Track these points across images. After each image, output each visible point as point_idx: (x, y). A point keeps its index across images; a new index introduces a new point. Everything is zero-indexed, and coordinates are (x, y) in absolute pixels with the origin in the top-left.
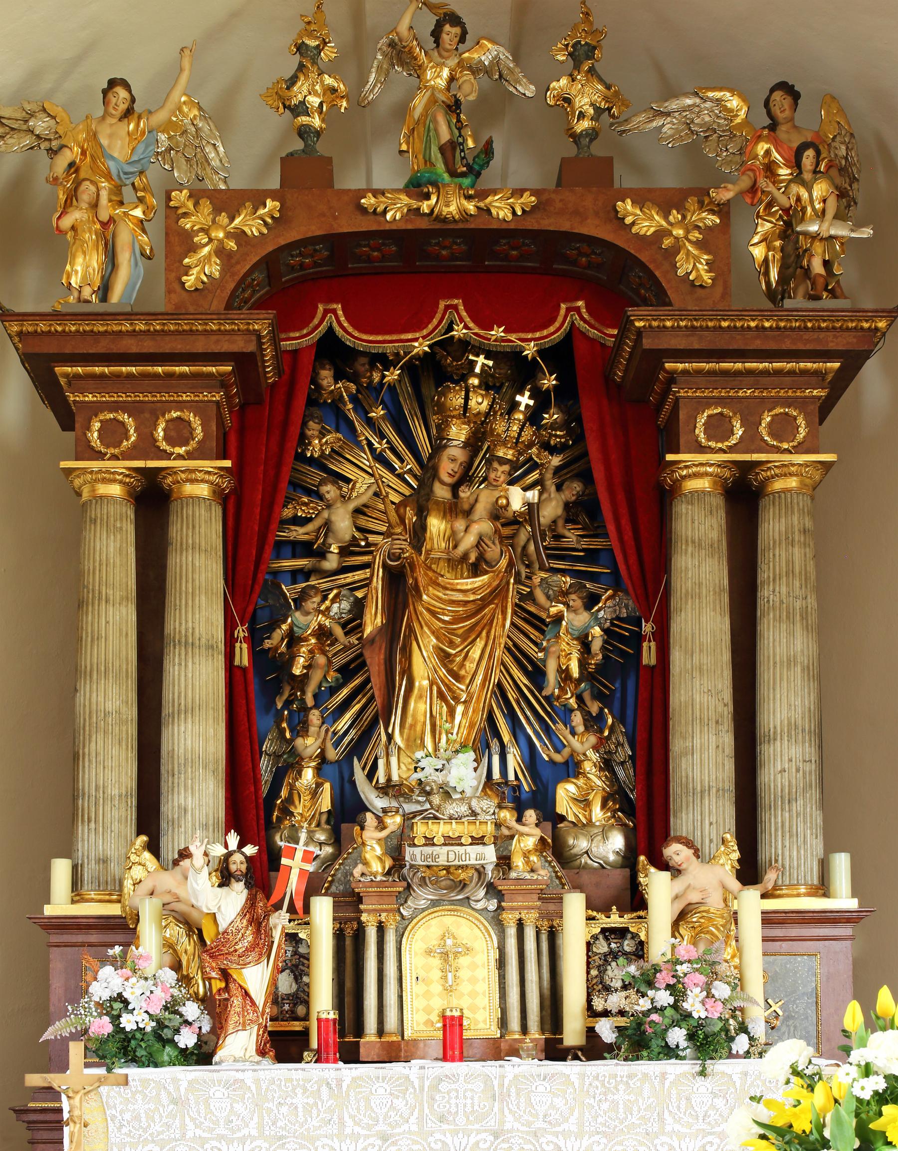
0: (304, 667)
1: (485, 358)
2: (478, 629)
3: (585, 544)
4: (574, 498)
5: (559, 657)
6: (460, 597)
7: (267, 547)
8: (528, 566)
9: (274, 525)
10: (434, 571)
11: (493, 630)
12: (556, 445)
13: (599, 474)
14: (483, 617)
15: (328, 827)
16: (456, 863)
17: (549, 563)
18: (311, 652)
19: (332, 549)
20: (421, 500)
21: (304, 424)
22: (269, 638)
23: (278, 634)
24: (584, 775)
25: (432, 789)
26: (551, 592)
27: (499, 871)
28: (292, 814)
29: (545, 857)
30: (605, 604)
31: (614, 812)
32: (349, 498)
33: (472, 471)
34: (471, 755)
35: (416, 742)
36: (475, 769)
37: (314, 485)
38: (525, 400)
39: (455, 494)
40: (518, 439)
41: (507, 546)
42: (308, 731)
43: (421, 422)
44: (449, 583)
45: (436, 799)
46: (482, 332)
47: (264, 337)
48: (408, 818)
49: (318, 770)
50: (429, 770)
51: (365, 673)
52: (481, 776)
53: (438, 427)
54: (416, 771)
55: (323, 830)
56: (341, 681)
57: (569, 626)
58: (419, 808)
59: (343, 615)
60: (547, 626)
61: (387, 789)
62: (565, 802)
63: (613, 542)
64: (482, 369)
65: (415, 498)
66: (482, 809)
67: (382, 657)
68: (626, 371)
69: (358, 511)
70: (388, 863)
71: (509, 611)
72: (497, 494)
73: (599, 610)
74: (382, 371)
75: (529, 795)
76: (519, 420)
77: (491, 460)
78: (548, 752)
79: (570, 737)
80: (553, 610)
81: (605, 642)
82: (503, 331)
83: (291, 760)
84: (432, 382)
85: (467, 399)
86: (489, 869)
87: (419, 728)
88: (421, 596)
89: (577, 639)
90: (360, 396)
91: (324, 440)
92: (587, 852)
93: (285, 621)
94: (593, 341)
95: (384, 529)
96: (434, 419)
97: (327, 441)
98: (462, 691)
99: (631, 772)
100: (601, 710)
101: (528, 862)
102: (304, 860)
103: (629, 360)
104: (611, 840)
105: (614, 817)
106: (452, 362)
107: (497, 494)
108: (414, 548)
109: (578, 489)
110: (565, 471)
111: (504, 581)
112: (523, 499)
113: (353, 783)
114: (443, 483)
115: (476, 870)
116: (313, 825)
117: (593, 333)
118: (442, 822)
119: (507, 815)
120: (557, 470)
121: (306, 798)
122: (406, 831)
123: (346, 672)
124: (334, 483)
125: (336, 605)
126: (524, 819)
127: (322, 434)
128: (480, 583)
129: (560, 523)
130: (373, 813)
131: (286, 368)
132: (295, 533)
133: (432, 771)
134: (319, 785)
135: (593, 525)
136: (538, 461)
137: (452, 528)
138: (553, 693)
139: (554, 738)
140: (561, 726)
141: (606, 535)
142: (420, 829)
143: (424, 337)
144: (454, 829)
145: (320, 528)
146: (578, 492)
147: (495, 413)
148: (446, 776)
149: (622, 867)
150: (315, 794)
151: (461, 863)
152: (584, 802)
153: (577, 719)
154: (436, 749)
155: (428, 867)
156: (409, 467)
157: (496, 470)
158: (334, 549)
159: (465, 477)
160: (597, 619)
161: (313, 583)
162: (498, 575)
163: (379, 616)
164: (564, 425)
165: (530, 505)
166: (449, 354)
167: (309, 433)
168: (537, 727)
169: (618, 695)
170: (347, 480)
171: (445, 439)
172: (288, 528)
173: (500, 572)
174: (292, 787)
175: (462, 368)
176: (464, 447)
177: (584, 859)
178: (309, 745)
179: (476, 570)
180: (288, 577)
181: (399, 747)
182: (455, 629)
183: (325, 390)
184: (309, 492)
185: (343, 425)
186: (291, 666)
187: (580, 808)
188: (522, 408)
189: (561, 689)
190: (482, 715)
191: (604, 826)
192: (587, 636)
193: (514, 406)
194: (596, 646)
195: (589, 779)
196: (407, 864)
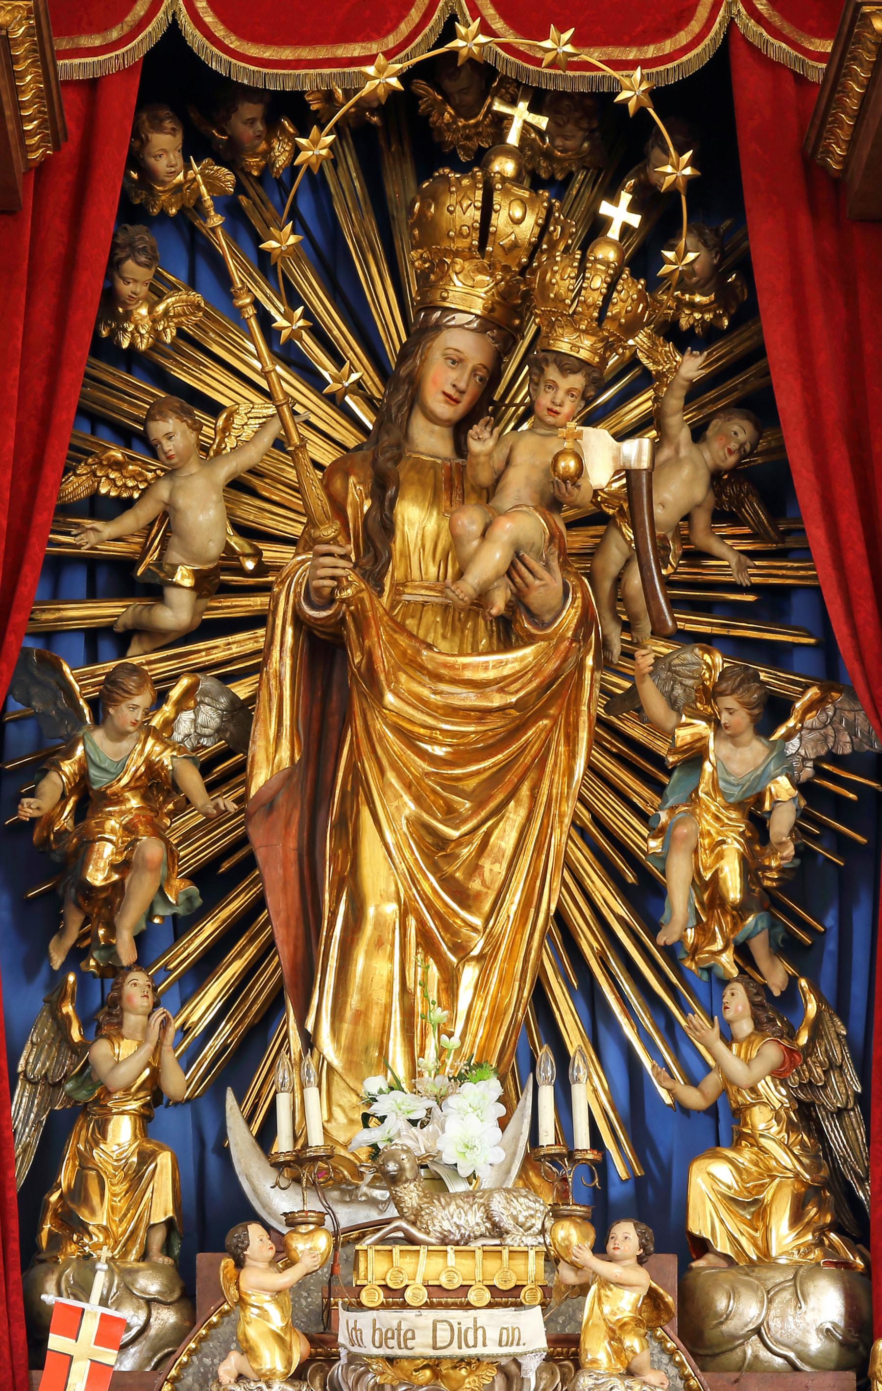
0: (114, 867)
1: (531, 109)
2: (511, 778)
3: (757, 573)
4: (732, 460)
5: (696, 851)
6: (468, 698)
7: (26, 569)
8: (626, 627)
9: (43, 516)
10: (411, 635)
11: (546, 783)
12: (692, 327)
13: (789, 401)
14: (523, 749)
15: (168, 1261)
16: (454, 1351)
17: (675, 620)
18: (129, 829)
19: (178, 578)
20: (383, 464)
21: (114, 266)
22: (32, 794)
23: (53, 785)
24: (753, 1140)
25: (402, 1169)
26: (678, 691)
27: (553, 1374)
28: (83, 1228)
29: (661, 1341)
30: (802, 721)
31: (822, 1231)
32: (218, 453)
33: (501, 389)
34: (492, 1087)
35: (367, 1055)
36: (503, 1123)
37: (137, 420)
38: (620, 213)
39: (460, 448)
40: (603, 310)
41: (576, 575)
42: (120, 1024)
43: (385, 267)
44: (445, 665)
45: (411, 1195)
46: (521, 43)
47: (18, 43)
48: (346, 1240)
49: (145, 1121)
50: (396, 1124)
51: (254, 882)
52: (516, 1139)
53: (423, 277)
54: (366, 1126)
55: (155, 1267)
56: (199, 902)
57: (720, 773)
58: (374, 1215)
59: (204, 741)
60: (669, 773)
61: (299, 1167)
62: (709, 1207)
63: (822, 571)
64: (523, 138)
65: (367, 452)
66: (515, 1218)
67: (292, 844)
68: (852, 144)
69: (238, 486)
70: (299, 1350)
71: (584, 736)
72: (554, 446)
73: (788, 737)
74: (291, 138)
75: (629, 1189)
76: (607, 264)
77: (540, 358)
78: (669, 1084)
79: (720, 1046)
80: (683, 736)
81: (803, 815)
82: (572, 41)
83: (82, 1096)
84: (409, 168)
85: (487, 209)
86: (531, 1366)
87: (375, 1021)
88: (380, 696)
89: (738, 806)
90: (244, 200)
91: (161, 308)
92: (757, 1331)
93: (68, 754)
94: (775, 67)
95: (297, 530)
96: (414, 259)
97: (166, 312)
98: (475, 929)
99: (861, 1133)
100: (792, 981)
101: (619, 1352)
102: (102, 1339)
103: (859, 117)
104: (812, 1301)
105: (820, 1243)
106: (455, 119)
107: (554, 446)
108: (365, 576)
109: (742, 437)
110: (712, 394)
111: (572, 660)
112: (616, 459)
113: (225, 1154)
114: (432, 418)
115: (501, 1369)
116: (132, 1257)
117: (778, 49)
118: (423, 1249)
119: (573, 1236)
120: (695, 392)
121: (116, 1188)
122: (341, 1270)
123: (213, 880)
124: (184, 414)
125: (187, 716)
126: (610, 1246)
127: (157, 294)
128: (517, 666)
129: (702, 520)
130: (268, 1228)
131: (71, 126)
132: (92, 538)
133: (403, 1125)
134: (146, 1158)
135: (776, 529)
136: (651, 367)
137: (451, 528)
138: (682, 941)
139: (685, 1049)
140: (699, 1019)
141: (805, 553)
142: (375, 1267)
143: (389, 55)
144: (451, 1268)
145: (151, 525)
146: (742, 445)
147: (553, 245)
148: (435, 1136)
149: (841, 1367)
150: (137, 1178)
151: (465, 1352)
152: (755, 1209)
153: (737, 1002)
154: (414, 1073)
155: (391, 1360)
156: (354, 377)
157: (554, 386)
158: (184, 577)
159: (485, 404)
160: (783, 757)
161: (136, 661)
162: (556, 647)
163: (285, 743)
164: (714, 280)
165: (629, 474)
166: (448, 99)
167: (126, 289)
168: (647, 1022)
169: (832, 945)
170: (214, 408)
171: (436, 308)
172: (78, 525)
173: (562, 639)
174: (85, 1164)
175: (479, 134)
176: (481, 330)
177: (752, 1348)
178: (123, 1058)
179: (506, 633)
180: (79, 645)
181: (330, 1067)
182: (458, 779)
183: (163, 183)
184: (127, 436)
185: (204, 273)
186: (84, 865)
187: (744, 1221)
188: (614, 233)
189: (702, 928)
190: (521, 990)
191: (798, 1266)
192: (759, 799)
193: (597, 227)
194: (782, 823)
195: (763, 1150)
196: (343, 1352)
